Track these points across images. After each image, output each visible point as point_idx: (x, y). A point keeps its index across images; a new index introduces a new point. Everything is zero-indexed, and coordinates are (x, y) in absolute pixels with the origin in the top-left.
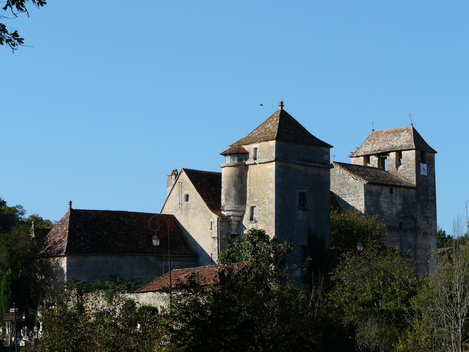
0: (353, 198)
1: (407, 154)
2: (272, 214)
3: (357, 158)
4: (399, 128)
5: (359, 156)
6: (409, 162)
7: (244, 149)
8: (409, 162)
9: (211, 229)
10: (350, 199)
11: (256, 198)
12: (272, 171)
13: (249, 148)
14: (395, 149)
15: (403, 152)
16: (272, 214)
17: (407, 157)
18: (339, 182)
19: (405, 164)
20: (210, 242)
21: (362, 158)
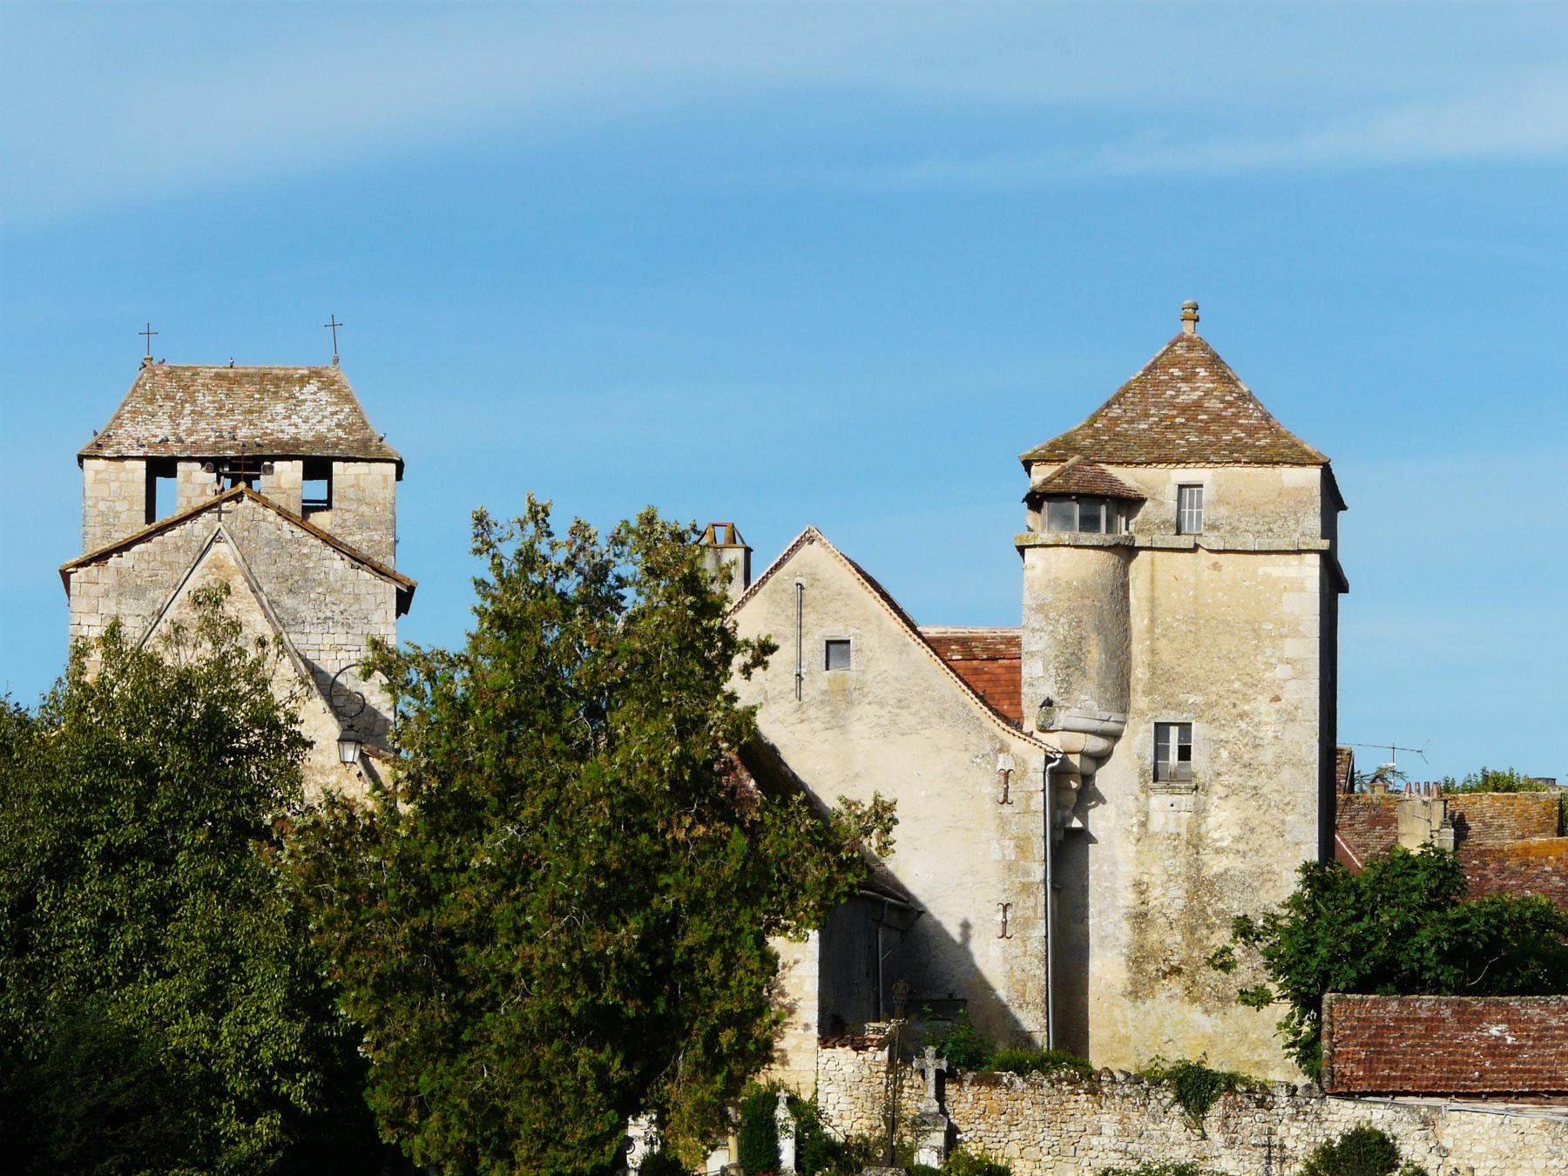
0: (341, 639)
1: (357, 476)
2: (1297, 764)
3: (114, 465)
4: (278, 366)
5: (123, 458)
6: (364, 509)
7: (1113, 481)
8: (364, 509)
9: (1005, 800)
10: (328, 640)
11: (1195, 689)
12: (1302, 589)
13: (1157, 482)
14: (305, 450)
15: (337, 466)
16: (1297, 764)
17: (356, 486)
18: (273, 569)
19: (347, 515)
20: (997, 856)
21: (143, 464)
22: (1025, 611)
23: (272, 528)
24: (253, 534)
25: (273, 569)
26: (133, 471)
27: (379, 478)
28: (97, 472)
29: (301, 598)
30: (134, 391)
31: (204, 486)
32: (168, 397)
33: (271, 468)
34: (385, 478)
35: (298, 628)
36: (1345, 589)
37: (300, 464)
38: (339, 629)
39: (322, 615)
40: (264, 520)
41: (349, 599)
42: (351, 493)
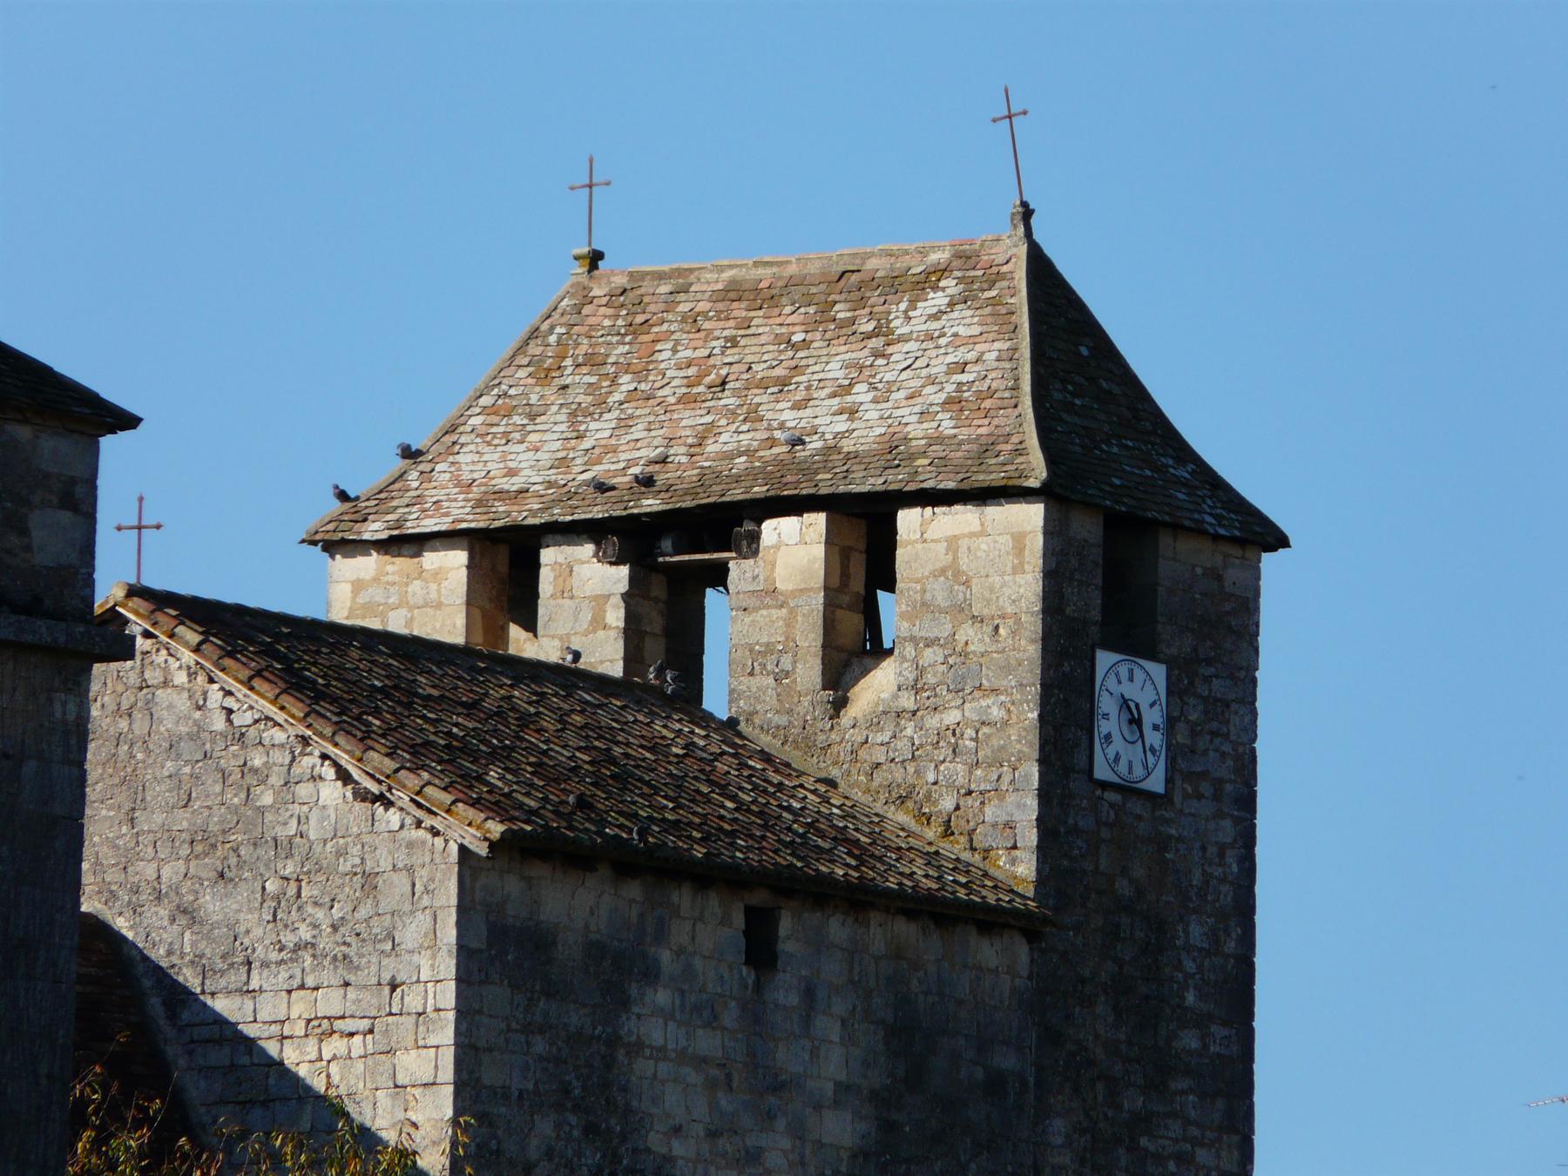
0: (330, 1002)
1: (952, 543)
3: (397, 566)
8: (967, 632)
10: (300, 1006)
14: (826, 484)
17: (954, 574)
18: (182, 820)
19: (930, 655)
21: (456, 561)
22: (158, 714)
23: (182, 703)
24: (140, 726)
25: (182, 820)
26: (438, 575)
27: (1005, 542)
28: (358, 586)
29: (243, 892)
30: (521, 349)
31: (601, 600)
32: (593, 361)
33: (755, 537)
34: (1019, 541)
35: (235, 978)
36: (890, 587)
37: (818, 520)
38: (329, 976)
39: (289, 939)
40: (166, 683)
41: (352, 889)
42: (939, 593)
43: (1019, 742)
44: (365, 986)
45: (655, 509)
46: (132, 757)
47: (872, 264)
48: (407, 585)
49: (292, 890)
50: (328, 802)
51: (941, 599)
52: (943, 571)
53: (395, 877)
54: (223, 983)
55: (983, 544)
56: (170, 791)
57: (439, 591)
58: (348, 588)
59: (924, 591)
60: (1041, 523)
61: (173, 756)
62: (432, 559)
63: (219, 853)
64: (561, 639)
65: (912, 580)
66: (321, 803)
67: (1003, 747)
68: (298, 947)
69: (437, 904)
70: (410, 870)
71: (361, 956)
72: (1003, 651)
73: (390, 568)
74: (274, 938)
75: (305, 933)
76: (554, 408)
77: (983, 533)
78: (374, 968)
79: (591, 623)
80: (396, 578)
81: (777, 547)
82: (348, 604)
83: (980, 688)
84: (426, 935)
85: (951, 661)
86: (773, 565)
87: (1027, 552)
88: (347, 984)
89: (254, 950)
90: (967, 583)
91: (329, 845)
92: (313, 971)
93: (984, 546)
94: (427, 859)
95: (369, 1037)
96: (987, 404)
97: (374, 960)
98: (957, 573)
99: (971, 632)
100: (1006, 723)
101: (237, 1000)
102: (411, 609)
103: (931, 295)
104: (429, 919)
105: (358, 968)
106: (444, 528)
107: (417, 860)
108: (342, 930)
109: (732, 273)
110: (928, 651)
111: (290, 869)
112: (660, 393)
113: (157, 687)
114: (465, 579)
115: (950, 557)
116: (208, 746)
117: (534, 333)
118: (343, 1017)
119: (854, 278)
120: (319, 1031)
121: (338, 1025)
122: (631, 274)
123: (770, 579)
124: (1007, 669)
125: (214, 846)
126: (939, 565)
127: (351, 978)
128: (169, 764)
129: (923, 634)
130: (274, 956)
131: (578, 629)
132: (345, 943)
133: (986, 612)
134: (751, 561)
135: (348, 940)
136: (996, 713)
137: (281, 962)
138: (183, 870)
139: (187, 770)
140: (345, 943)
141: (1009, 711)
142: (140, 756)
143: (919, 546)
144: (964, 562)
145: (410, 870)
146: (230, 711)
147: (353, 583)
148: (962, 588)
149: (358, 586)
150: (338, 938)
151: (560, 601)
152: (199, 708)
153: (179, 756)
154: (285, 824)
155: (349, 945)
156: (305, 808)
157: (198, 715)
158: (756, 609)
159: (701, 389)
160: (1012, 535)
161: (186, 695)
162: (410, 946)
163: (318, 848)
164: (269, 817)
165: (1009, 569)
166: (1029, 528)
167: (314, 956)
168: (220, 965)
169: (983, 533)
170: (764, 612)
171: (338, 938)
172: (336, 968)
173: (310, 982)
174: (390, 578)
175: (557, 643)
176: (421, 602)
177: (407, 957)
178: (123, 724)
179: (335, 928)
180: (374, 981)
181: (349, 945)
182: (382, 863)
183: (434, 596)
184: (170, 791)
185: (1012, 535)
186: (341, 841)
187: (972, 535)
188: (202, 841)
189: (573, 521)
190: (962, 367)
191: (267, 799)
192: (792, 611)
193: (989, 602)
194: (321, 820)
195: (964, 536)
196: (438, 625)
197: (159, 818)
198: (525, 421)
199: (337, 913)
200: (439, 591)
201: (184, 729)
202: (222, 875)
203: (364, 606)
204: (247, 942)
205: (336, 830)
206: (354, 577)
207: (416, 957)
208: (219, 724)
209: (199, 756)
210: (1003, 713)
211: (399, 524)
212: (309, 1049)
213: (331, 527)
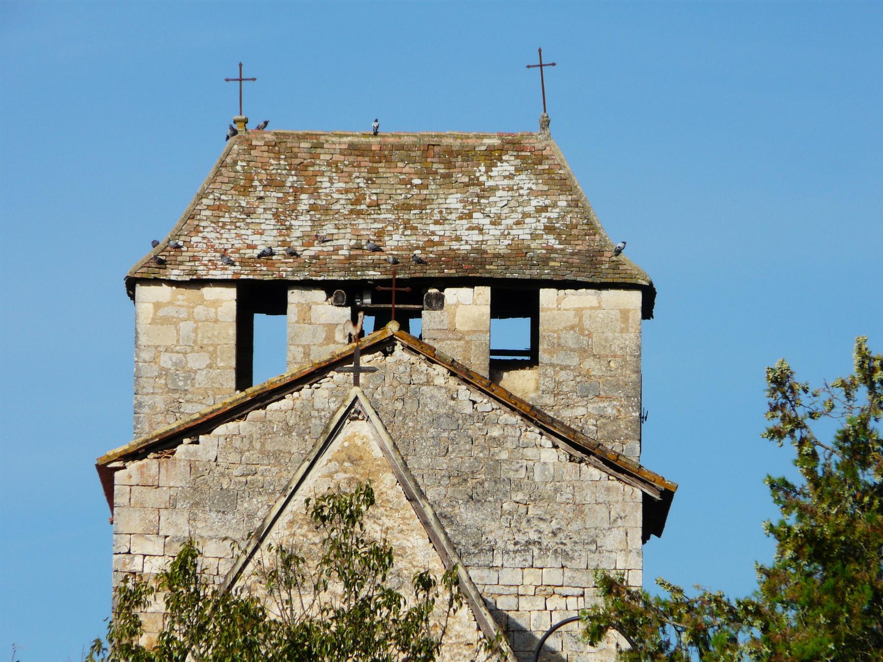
0: (553, 576)
1: (579, 312)
3: (184, 294)
10: (531, 578)
14: (494, 270)
17: (577, 328)
18: (443, 463)
19: (563, 375)
21: (231, 293)
23: (441, 395)
24: (410, 406)
25: (443, 463)
26: (216, 303)
27: (615, 314)
28: (157, 306)
29: (488, 508)
30: (218, 173)
31: (331, 328)
33: (440, 299)
35: (483, 559)
38: (550, 561)
40: (428, 383)
42: (569, 339)
43: (627, 429)
44: (577, 569)
45: (376, 278)
46: (404, 423)
47: (446, 141)
48: (193, 307)
49: (522, 509)
50: (547, 460)
51: (571, 344)
52: (572, 328)
53: (597, 507)
54: (475, 560)
55: (600, 314)
56: (434, 446)
57: (216, 313)
58: (151, 306)
59: (559, 338)
60: (640, 305)
61: (435, 425)
62: (209, 292)
63: (469, 485)
64: (304, 347)
65: (550, 331)
66: (542, 461)
67: (615, 431)
68: (528, 543)
69: (627, 525)
70: (608, 504)
71: (574, 551)
72: (615, 376)
73: (180, 297)
74: (511, 537)
75: (534, 536)
76: (260, 210)
77: (600, 308)
78: (584, 559)
79: (325, 339)
80: (185, 303)
81: (456, 305)
82: (151, 316)
83: (598, 396)
84: (620, 542)
85: (578, 379)
86: (454, 316)
87: (630, 321)
88: (563, 567)
89: (496, 543)
90: (590, 335)
91: (548, 485)
92: (540, 558)
93: (600, 315)
94: (620, 498)
95: (581, 599)
96: (574, 232)
97: (584, 554)
98: (582, 330)
99: (593, 364)
100: (616, 418)
101: (486, 572)
102: (196, 322)
103: (499, 164)
104: (623, 534)
105: (572, 558)
106: (225, 277)
107: (612, 498)
108: (561, 535)
109: (349, 139)
110: (563, 373)
111: (519, 497)
112: (334, 207)
113: (423, 385)
114: (235, 308)
115: (577, 320)
116: (460, 422)
117: (223, 164)
118: (562, 586)
119: (437, 149)
120: (545, 593)
121: (557, 590)
122: (276, 134)
123: (452, 323)
124: (617, 387)
125: (465, 480)
126: (569, 324)
127: (568, 564)
128: (432, 430)
129: (559, 362)
130: (511, 547)
131: (316, 342)
132: (562, 543)
133: (602, 352)
134: (439, 312)
135: (564, 541)
136: (610, 411)
137: (515, 552)
138: (444, 492)
139: (446, 434)
140: (562, 543)
141: (619, 411)
142: (410, 424)
143: (556, 312)
144: (587, 323)
145: (608, 504)
146: (474, 402)
147: (154, 304)
148: (586, 338)
149: (157, 306)
150: (557, 540)
151: (302, 325)
152: (453, 399)
153: (439, 426)
154: (517, 471)
155: (565, 544)
156: (531, 463)
157: (452, 403)
158: (443, 340)
159: (363, 207)
160: (620, 310)
161: (443, 391)
162: (609, 548)
163: (541, 487)
164: (504, 466)
165: (618, 329)
166: (632, 308)
167: (540, 549)
168: (473, 550)
169: (600, 308)
170: (448, 342)
171: (557, 540)
172: (556, 557)
173: (538, 563)
174: (180, 303)
175: (301, 349)
176: (204, 319)
177: (608, 554)
178: (399, 405)
179: (554, 534)
180: (584, 566)
181: (565, 544)
182: (588, 498)
183: (212, 315)
184: (434, 446)
185: (620, 310)
186: (558, 484)
187: (592, 308)
188: (459, 477)
189: (324, 280)
190: (544, 209)
191: (504, 455)
192: (467, 342)
193: (605, 347)
194: (543, 472)
195: (586, 308)
196: (216, 333)
197: (425, 461)
198: (244, 217)
199: (554, 525)
200: (216, 313)
201: (442, 411)
202: (471, 497)
203: (161, 318)
204: (490, 538)
205: (554, 477)
206: (155, 300)
207: (613, 555)
208: (469, 410)
209: (454, 427)
210: (615, 412)
211: (193, 272)
212: (538, 603)
213: (144, 270)
